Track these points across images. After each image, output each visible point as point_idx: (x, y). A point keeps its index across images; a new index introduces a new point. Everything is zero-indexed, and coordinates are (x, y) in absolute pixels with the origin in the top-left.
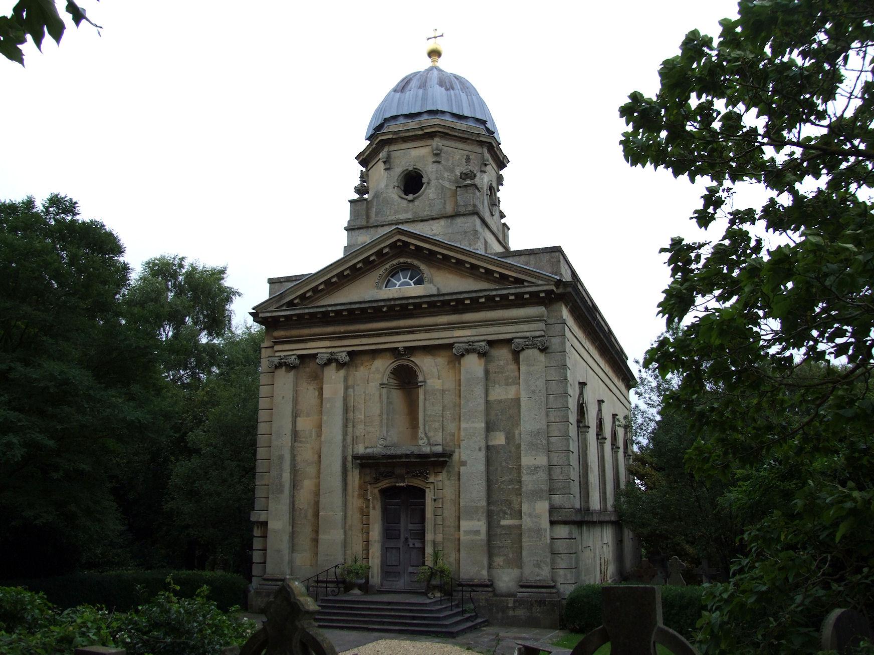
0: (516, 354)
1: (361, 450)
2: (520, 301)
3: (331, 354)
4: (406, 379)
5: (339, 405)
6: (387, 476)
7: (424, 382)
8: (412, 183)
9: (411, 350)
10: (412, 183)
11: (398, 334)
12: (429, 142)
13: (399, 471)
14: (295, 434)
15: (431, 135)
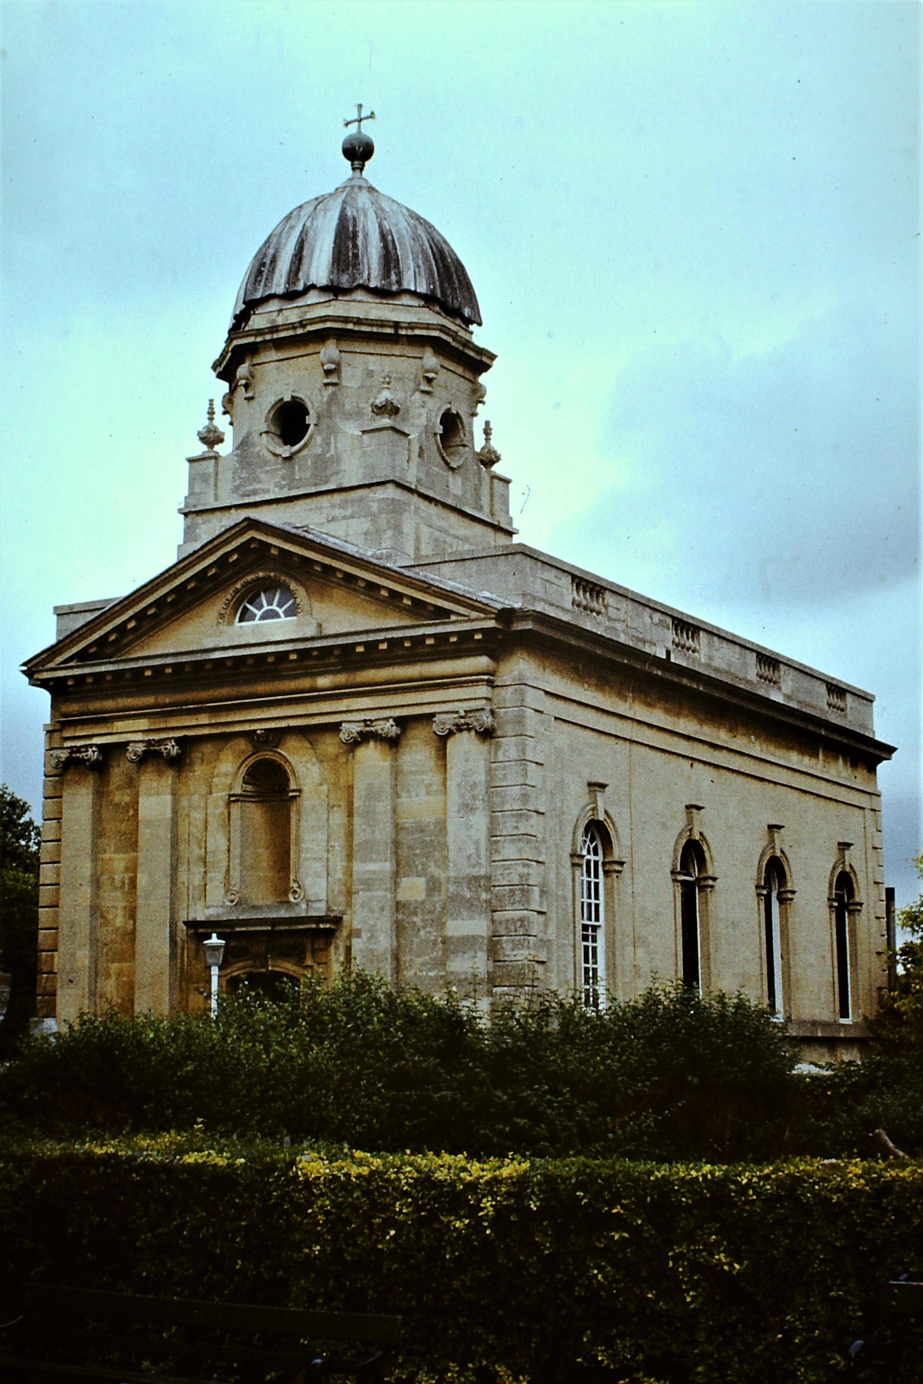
0: (443, 741)
2: (444, 648)
3: (149, 743)
4: (270, 787)
7: (300, 791)
8: (290, 421)
9: (277, 736)
10: (290, 421)
15: (321, 337)
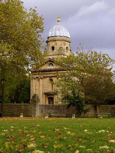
1: (45, 92)
5: (42, 85)
6: (49, 95)
9: (52, 77)
11: (47, 74)
12: (55, 41)
13: (50, 95)
14: (36, 89)
